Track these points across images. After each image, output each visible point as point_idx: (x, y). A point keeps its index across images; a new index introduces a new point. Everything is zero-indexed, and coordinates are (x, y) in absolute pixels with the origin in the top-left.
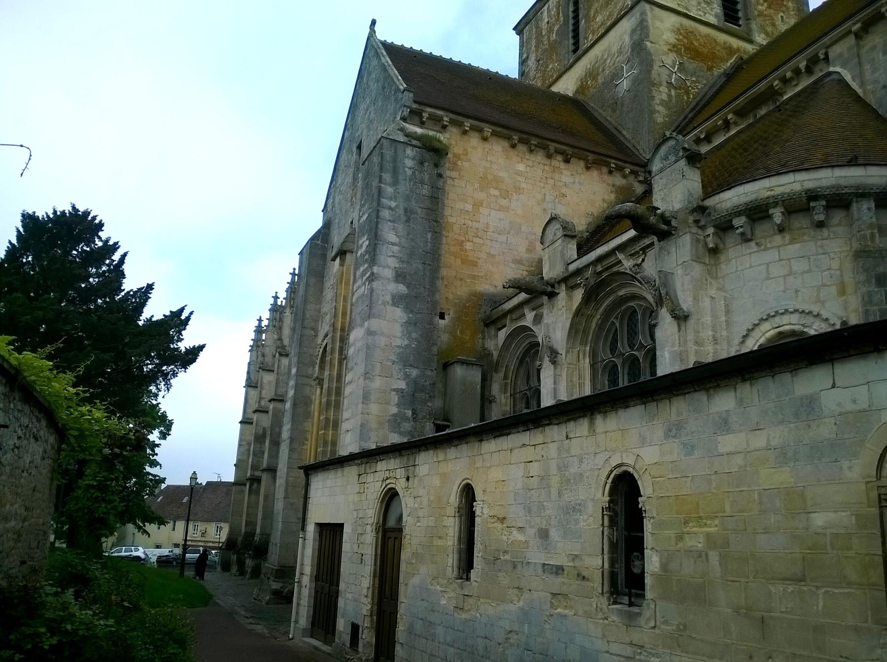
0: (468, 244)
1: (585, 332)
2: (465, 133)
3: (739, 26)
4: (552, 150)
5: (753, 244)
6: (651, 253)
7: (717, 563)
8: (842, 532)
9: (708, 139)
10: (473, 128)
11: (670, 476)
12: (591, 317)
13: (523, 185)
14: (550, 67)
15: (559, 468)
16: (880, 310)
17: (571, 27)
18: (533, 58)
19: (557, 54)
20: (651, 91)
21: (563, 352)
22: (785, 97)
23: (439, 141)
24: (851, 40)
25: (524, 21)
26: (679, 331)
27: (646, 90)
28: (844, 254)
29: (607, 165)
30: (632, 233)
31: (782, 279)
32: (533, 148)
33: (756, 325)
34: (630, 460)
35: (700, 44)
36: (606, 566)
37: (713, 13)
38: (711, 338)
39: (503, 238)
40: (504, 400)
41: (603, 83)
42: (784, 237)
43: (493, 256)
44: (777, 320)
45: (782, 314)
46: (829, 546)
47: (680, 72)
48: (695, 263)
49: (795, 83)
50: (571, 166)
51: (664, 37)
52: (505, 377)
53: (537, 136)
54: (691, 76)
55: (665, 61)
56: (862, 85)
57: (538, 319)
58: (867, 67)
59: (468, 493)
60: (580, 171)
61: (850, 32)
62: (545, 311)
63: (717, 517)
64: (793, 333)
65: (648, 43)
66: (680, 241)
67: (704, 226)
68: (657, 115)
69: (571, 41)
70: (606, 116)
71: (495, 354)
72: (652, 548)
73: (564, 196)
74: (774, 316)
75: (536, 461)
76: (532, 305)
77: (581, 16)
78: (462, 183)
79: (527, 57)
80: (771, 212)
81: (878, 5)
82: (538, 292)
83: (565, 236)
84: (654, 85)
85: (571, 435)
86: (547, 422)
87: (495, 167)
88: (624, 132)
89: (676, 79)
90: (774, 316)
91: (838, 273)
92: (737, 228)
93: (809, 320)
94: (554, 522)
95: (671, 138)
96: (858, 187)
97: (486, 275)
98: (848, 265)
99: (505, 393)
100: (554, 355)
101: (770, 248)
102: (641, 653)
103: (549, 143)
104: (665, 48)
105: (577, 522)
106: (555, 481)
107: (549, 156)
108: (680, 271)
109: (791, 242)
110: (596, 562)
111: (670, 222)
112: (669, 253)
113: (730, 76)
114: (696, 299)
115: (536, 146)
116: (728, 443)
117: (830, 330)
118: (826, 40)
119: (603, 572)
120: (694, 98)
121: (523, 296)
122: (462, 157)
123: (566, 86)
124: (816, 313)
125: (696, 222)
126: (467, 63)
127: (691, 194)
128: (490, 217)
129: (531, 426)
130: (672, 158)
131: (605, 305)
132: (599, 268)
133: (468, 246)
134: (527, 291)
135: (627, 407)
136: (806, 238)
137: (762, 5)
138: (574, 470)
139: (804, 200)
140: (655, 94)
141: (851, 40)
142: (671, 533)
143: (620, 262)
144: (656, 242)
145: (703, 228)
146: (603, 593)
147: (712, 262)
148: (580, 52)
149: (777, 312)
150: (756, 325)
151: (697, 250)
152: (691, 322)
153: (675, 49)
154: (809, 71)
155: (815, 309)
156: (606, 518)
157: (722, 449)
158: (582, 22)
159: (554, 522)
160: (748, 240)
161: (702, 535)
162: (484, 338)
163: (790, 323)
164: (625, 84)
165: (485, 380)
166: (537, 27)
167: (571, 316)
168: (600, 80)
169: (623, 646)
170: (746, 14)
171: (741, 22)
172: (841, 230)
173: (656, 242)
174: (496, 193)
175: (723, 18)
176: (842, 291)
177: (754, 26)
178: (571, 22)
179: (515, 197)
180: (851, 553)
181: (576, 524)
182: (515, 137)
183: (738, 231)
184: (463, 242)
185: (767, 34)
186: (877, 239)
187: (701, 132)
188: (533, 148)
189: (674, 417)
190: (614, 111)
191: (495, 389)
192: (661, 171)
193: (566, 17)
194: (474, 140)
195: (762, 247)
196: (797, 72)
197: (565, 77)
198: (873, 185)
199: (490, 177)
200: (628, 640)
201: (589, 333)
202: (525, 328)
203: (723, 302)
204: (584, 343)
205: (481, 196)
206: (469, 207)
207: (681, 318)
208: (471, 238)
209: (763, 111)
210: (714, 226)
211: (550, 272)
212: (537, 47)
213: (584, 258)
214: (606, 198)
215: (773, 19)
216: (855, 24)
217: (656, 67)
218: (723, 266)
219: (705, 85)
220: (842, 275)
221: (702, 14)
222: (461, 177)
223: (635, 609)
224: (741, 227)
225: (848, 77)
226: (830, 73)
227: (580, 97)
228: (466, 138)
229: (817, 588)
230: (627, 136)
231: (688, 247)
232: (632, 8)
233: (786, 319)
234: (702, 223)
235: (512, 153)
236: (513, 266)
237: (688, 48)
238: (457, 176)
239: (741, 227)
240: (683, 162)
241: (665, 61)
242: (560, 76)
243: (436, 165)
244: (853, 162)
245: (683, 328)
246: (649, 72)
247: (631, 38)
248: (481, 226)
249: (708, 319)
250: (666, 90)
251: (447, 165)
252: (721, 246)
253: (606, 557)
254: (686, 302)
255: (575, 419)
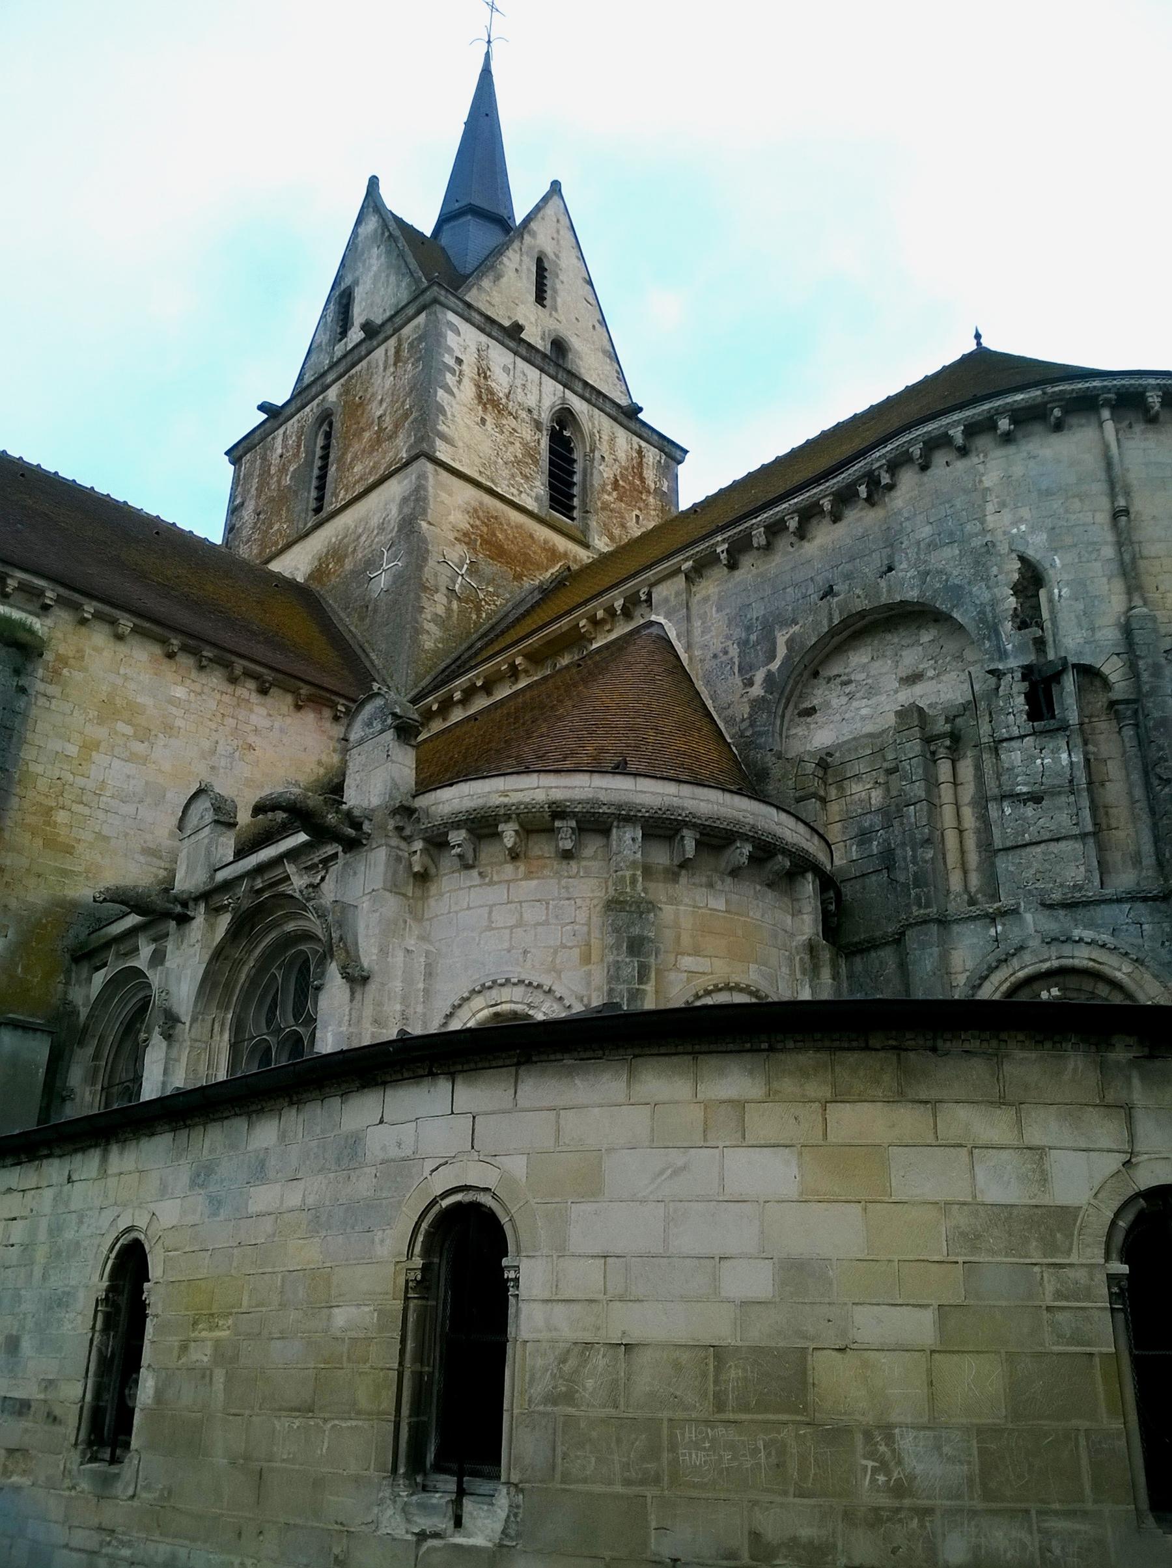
0: (62, 812)
1: (229, 987)
2: (83, 622)
3: (573, 519)
4: (238, 671)
5: (474, 873)
6: (335, 869)
7: (222, 1386)
8: (362, 1335)
9: (487, 689)
10: (98, 616)
11: (187, 1249)
12: (241, 962)
13: (179, 723)
14: (276, 527)
15: (50, 1231)
16: (629, 990)
17: (316, 472)
18: (250, 506)
19: (288, 510)
20: (418, 598)
21: (186, 1019)
22: (595, 646)
23: (30, 631)
24: (680, 581)
25: (244, 444)
26: (351, 1001)
27: (412, 595)
28: (595, 902)
29: (333, 706)
30: (302, 837)
31: (508, 931)
32: (204, 663)
33: (465, 1000)
34: (142, 1223)
35: (507, 538)
36: (89, 1397)
37: (533, 494)
38: (398, 1016)
39: (129, 809)
40: (88, 1097)
41: (352, 572)
42: (517, 868)
43: (106, 839)
44: (494, 996)
45: (502, 985)
46: (345, 1358)
47: (470, 577)
48: (388, 894)
49: (607, 627)
50: (269, 700)
51: (451, 518)
52: (96, 1057)
53: (214, 645)
54: (488, 584)
55: (448, 556)
56: (689, 647)
57: (158, 958)
58: (697, 623)
59: (130, 1262)
60: (284, 709)
61: (677, 571)
62: (170, 946)
63: (231, 1314)
64: (515, 1015)
65: (424, 524)
66: (372, 856)
67: (410, 837)
68: (425, 637)
69: (314, 494)
70: (350, 624)
71: (84, 1012)
72: (149, 1366)
73: (251, 747)
74: (490, 988)
75: (22, 1218)
76: (152, 932)
77: (331, 459)
78: (67, 707)
79: (242, 504)
80: (500, 829)
81: (712, 542)
82: (161, 911)
83: (217, 822)
84: (425, 589)
85: (74, 1178)
86: (45, 1152)
87: (132, 686)
88: (373, 656)
89: (462, 585)
90: (490, 988)
91: (585, 928)
92: (454, 847)
93: (537, 997)
94: (30, 1323)
95: (378, 694)
96: (620, 807)
97: (87, 871)
98: (596, 920)
99: (93, 1084)
100: (171, 1019)
101: (496, 883)
102: (109, 1543)
103: (234, 658)
104: (451, 536)
105: (60, 1321)
106: (41, 1254)
107: (233, 680)
108: (365, 905)
109: (529, 876)
110: (74, 1393)
111: (361, 824)
112: (355, 873)
113: (548, 592)
114: (384, 951)
115: (210, 660)
116: (263, 1198)
117: (563, 1015)
118: (650, 574)
119: (82, 1408)
120: (489, 618)
121: (133, 920)
122: (72, 662)
123: (295, 564)
124: (546, 988)
125: (400, 829)
126: (122, 500)
127: (395, 786)
128: (111, 772)
129: (24, 1158)
130: (377, 726)
131: (263, 944)
132: (259, 884)
133: (61, 817)
134: (137, 909)
135: (153, 1134)
136: (546, 872)
137: (609, 494)
138: (69, 1235)
139: (547, 815)
140: (425, 603)
141: (680, 581)
142: (174, 1340)
143: (288, 878)
144: (341, 854)
145: (408, 840)
146: (76, 1444)
147: (419, 893)
148: (323, 514)
149: (494, 982)
150: (465, 1000)
151: (395, 872)
152: (372, 987)
153: (467, 540)
154: (627, 614)
155: (547, 982)
156: (100, 1316)
157: (253, 1208)
158: (332, 469)
159: (30, 1323)
160: (468, 867)
161: (209, 1343)
162: (67, 983)
163: (511, 1001)
164: (382, 581)
165: (57, 1062)
166: (264, 458)
167: (207, 958)
168: (348, 565)
169: (87, 1532)
170: (584, 503)
171: (575, 514)
172: (595, 865)
173: (341, 854)
174: (129, 730)
175: (547, 503)
176: (586, 959)
177: (593, 524)
178: (318, 463)
179: (161, 740)
180: (365, 1368)
181: (59, 1327)
182: (175, 642)
183: (453, 852)
184: (51, 809)
185: (612, 538)
186: (639, 887)
187: (477, 676)
188: (204, 663)
189: (206, 1155)
190: (362, 619)
191: (76, 1076)
192: (361, 742)
193: (310, 453)
194: (99, 637)
195: (487, 880)
196: (611, 611)
197: (296, 549)
198: (643, 806)
199: (118, 701)
200: (95, 1521)
201: (234, 987)
202: (137, 972)
203: (422, 959)
204: (223, 1006)
205: (100, 732)
206: (73, 750)
207: (357, 979)
208: (68, 803)
209: (565, 661)
210: (424, 839)
211: (188, 881)
212: (260, 490)
213: (241, 863)
214: (324, 758)
215: (622, 518)
216: (686, 560)
217: (431, 563)
218: (432, 902)
219: (508, 600)
220: (589, 933)
221: (515, 492)
222: (65, 697)
223: (114, 1469)
224: (459, 845)
225: (672, 635)
226: (652, 624)
227: (315, 586)
228: (84, 630)
229: (325, 1420)
230: (376, 662)
231: (381, 868)
232: (407, 464)
233: (506, 993)
234: (407, 832)
235: (167, 666)
236: (142, 859)
237: (486, 541)
238: (58, 695)
239: (459, 845)
240: (390, 735)
241: (448, 556)
242: (288, 546)
243: (17, 672)
244: (620, 769)
245: (358, 996)
246: (420, 568)
247: (400, 512)
248: (90, 785)
249: (397, 985)
250: (445, 601)
251: (40, 672)
252: (433, 871)
253: (89, 1386)
254: (368, 955)
255: (83, 1150)
